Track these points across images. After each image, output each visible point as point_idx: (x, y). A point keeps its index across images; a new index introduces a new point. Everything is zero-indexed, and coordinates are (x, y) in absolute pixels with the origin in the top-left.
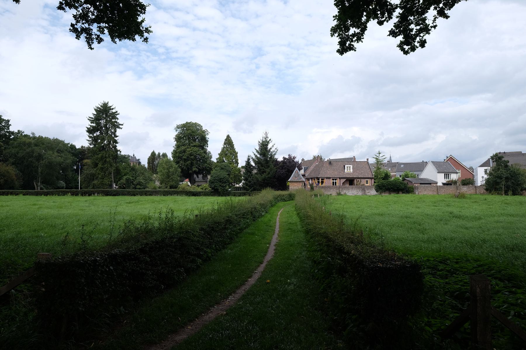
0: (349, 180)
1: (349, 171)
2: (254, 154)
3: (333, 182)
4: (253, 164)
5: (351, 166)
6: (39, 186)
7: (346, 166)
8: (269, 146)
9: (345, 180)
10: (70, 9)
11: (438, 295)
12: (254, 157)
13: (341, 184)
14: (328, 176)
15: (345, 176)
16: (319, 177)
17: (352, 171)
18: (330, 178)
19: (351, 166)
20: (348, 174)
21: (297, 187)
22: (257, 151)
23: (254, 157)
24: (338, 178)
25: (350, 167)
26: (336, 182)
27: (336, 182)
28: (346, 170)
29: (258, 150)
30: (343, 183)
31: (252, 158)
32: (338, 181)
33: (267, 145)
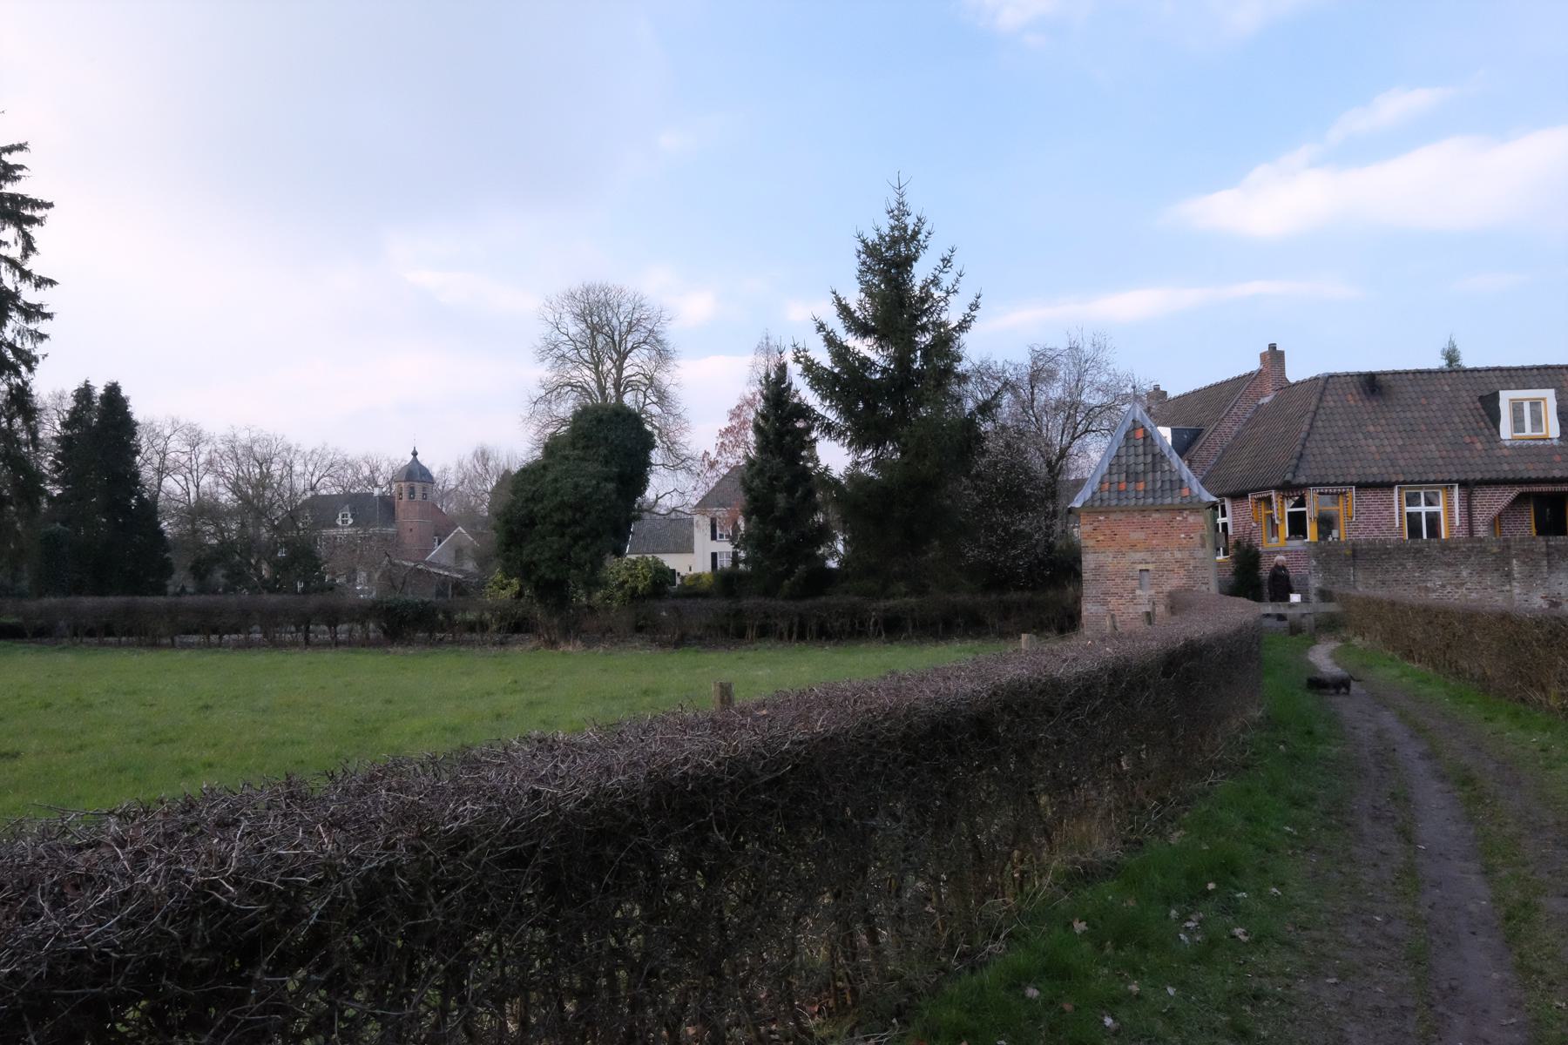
0: (1538, 496)
1: (1528, 432)
2: (831, 341)
3: (1414, 520)
4: (808, 396)
5: (1549, 395)
6: (750, 633)
7: (1506, 398)
8: (921, 272)
9: (1510, 494)
10: (113, 391)
11: (17, 532)
12: (824, 358)
13: (1482, 531)
14: (1374, 472)
15: (1505, 470)
16: (1302, 480)
17: (1552, 428)
18: (1389, 486)
19: (1549, 395)
20: (1524, 451)
21: (1147, 556)
22: (844, 311)
23: (824, 358)
24: (1351, 484)
25: (1535, 404)
26: (1433, 520)
27: (1437, 514)
28: (1506, 430)
29: (853, 306)
30: (1497, 522)
31: (810, 368)
32: (1450, 510)
33: (908, 261)
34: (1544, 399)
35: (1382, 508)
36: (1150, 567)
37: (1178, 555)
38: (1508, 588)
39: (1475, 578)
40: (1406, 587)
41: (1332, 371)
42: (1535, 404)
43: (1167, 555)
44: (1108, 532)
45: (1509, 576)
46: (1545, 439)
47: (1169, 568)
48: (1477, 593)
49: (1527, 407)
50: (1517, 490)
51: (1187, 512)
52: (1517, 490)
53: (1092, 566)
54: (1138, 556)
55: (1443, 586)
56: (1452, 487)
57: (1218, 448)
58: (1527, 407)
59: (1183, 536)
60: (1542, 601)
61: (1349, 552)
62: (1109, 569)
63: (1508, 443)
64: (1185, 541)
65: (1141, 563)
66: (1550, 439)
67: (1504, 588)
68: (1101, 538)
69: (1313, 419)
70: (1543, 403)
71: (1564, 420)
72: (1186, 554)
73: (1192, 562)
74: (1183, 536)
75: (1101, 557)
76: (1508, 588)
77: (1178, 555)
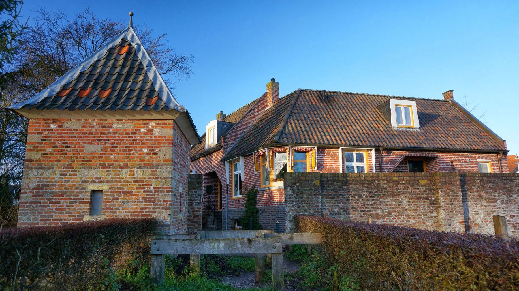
1: (404, 124)
15: (398, 142)
34: (410, 106)
35: (332, 162)
36: (104, 187)
37: (139, 174)
38: (435, 214)
39: (412, 207)
40: (362, 214)
41: (303, 88)
42: (407, 108)
43: (125, 173)
44: (58, 143)
45: (435, 204)
46: (412, 128)
47: (126, 189)
48: (414, 218)
49: (403, 108)
50: (404, 154)
51: (153, 123)
52: (404, 154)
53: (33, 185)
54: (92, 173)
55: (390, 213)
56: (371, 150)
57: (241, 132)
58: (403, 108)
59: (146, 151)
60: (461, 225)
61: (317, 182)
62: (55, 189)
63: (396, 129)
64: (147, 158)
65: (95, 182)
66: (415, 128)
67: (433, 215)
68: (49, 150)
69: (293, 109)
70: (410, 108)
71: (422, 120)
72: (148, 173)
73: (154, 183)
74: (146, 151)
75: (46, 174)
76: (435, 214)
77: (139, 174)
